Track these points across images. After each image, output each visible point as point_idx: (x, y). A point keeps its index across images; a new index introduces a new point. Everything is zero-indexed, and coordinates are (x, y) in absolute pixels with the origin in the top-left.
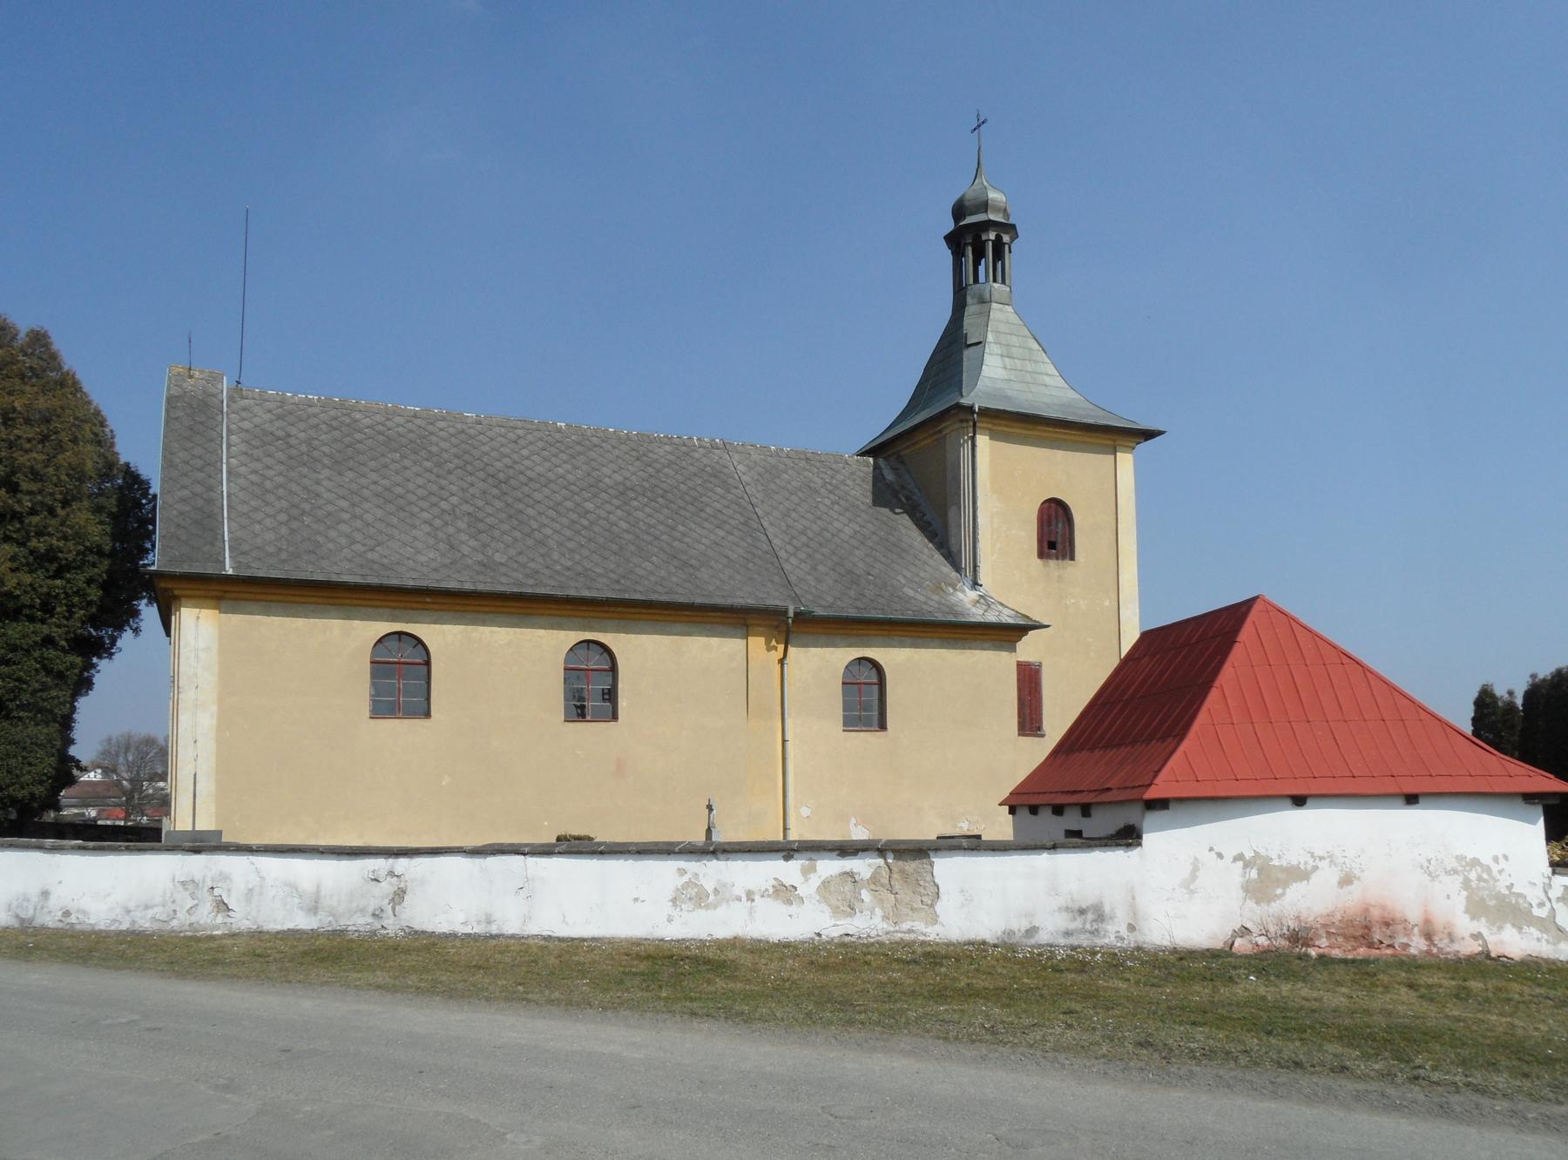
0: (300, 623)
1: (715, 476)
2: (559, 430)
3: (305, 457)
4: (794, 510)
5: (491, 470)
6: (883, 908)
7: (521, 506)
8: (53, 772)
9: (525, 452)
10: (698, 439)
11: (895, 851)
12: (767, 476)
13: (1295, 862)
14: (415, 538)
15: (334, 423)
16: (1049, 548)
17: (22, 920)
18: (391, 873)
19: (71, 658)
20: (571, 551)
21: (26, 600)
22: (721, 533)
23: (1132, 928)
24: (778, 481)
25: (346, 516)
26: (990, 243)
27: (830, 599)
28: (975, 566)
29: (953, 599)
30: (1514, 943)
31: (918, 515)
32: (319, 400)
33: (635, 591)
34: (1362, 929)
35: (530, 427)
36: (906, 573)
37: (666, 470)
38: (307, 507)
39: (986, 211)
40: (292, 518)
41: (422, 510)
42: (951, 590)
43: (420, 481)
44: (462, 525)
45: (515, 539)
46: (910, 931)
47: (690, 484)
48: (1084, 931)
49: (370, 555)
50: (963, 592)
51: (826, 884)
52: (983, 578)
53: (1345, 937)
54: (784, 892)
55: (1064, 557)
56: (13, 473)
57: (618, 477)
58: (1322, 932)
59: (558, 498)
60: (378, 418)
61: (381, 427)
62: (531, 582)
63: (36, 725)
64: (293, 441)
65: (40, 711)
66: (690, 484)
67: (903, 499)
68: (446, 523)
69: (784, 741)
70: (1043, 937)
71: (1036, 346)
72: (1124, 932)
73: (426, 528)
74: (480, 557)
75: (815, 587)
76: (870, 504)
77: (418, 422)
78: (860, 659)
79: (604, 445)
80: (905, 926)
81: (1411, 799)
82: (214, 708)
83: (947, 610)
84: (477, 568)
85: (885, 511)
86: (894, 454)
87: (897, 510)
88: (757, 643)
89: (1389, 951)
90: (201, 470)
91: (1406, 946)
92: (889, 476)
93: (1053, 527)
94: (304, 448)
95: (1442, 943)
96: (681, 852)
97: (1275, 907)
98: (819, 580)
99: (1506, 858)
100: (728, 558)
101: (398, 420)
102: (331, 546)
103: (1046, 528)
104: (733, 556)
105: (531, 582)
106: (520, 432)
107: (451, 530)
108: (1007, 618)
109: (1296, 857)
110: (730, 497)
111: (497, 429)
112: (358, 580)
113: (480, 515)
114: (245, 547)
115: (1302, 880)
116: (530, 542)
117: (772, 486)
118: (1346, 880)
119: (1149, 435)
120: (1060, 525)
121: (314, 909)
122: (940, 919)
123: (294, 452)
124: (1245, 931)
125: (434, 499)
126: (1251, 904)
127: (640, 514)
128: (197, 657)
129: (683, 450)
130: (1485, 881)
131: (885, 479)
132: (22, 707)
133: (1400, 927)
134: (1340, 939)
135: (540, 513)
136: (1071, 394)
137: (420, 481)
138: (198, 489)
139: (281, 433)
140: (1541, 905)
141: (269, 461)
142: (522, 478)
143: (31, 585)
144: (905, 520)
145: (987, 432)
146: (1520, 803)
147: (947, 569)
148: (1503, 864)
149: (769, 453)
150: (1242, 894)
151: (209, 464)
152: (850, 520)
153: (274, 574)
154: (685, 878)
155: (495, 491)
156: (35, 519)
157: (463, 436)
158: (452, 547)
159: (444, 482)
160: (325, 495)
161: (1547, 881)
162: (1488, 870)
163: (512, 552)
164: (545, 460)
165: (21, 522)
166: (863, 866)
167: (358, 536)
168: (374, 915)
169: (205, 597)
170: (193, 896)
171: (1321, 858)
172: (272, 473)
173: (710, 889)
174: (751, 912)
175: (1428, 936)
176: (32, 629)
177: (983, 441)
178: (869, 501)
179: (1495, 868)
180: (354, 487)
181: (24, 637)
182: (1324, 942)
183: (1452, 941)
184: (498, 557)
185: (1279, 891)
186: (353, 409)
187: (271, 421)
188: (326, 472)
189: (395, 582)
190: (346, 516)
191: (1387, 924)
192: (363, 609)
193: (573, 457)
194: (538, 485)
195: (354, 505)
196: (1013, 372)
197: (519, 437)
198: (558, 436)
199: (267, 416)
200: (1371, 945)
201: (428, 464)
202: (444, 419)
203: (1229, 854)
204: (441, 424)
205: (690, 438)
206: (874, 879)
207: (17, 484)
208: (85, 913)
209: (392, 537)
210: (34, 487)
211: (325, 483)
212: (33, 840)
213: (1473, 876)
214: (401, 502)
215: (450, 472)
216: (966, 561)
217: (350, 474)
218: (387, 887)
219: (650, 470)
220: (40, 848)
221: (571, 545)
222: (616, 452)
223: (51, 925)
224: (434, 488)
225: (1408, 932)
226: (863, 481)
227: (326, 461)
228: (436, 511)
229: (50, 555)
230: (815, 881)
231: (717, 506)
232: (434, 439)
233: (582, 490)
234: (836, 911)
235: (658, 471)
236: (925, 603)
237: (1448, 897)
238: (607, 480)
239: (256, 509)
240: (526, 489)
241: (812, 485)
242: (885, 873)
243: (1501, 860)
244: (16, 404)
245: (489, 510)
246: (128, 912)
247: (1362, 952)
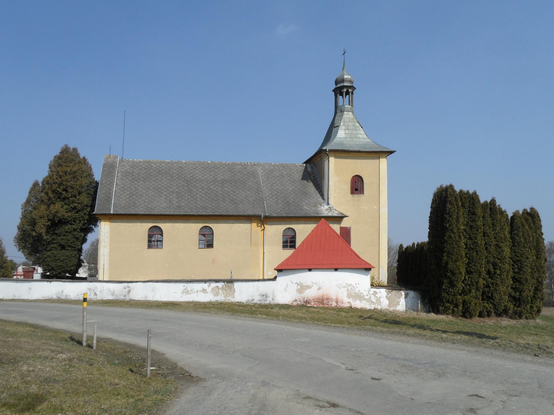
0: (130, 224)
1: (252, 175)
2: (208, 164)
3: (137, 179)
4: (275, 183)
5: (186, 178)
6: (224, 294)
7: (192, 188)
8: (76, 264)
9: (197, 172)
10: (250, 163)
11: (227, 281)
12: (269, 173)
13: (308, 284)
14: (161, 200)
15: (146, 167)
16: (355, 191)
17: (58, 297)
18: (128, 287)
19: (79, 234)
20: (203, 201)
21: (70, 219)
22: (249, 193)
23: (273, 299)
24: (272, 174)
25: (144, 195)
26: (345, 93)
27: (279, 211)
29: (319, 209)
30: (358, 304)
31: (316, 182)
32: (143, 161)
33: (218, 212)
34: (321, 300)
35: (200, 163)
36: (306, 201)
37: (238, 174)
38: (135, 193)
39: (344, 82)
40: (130, 196)
41: (165, 191)
42: (320, 206)
43: (166, 183)
44: (175, 195)
45: (188, 199)
46: (229, 300)
47: (244, 178)
48: (263, 300)
49: (148, 206)
50: (324, 206)
51: (213, 289)
53: (318, 302)
54: (204, 291)
55: (360, 193)
56: (66, 188)
57: (222, 177)
58: (313, 301)
59: (203, 185)
60: (158, 165)
61: (158, 168)
62: (189, 211)
63: (72, 251)
64: (134, 174)
65: (73, 247)
66: (244, 178)
67: (312, 177)
68: (170, 195)
69: (264, 253)
70: (255, 302)
71: (358, 125)
72: (271, 300)
73: (165, 197)
74: (177, 204)
75: (276, 207)
76: (301, 179)
77: (169, 165)
78: (289, 228)
79: (221, 167)
80: (228, 299)
81: (336, 270)
82: (109, 247)
83: (316, 212)
84: (176, 208)
85: (305, 181)
86: (312, 162)
87: (309, 181)
88: (254, 225)
89: (327, 306)
90: (109, 185)
91: (331, 304)
92: (309, 169)
93: (357, 184)
94: (137, 176)
95: (340, 304)
96: (183, 282)
97: (302, 295)
98: (277, 205)
99: (359, 284)
100: (249, 200)
101: (164, 165)
102: (139, 204)
103: (354, 184)
104: (250, 199)
105: (189, 211)
106: (197, 165)
107: (171, 197)
108: (335, 214)
109: (308, 283)
110: (255, 181)
111: (190, 165)
112: (144, 213)
113: (180, 192)
114: (117, 205)
115: (309, 288)
116: (192, 199)
117: (270, 176)
118: (319, 289)
119: (391, 152)
120: (359, 183)
121: (113, 295)
122: (235, 297)
123: (134, 177)
124: (296, 300)
125: (168, 188)
126: (298, 294)
127: (226, 188)
128: (104, 234)
129: (244, 166)
130: (353, 289)
131: (307, 171)
132: (69, 246)
133: (330, 300)
134: (317, 303)
135: (197, 190)
136: (368, 140)
137: (166, 183)
138: (108, 190)
139: (131, 172)
140: (367, 295)
141: (127, 180)
142: (195, 180)
143: (71, 216)
144: (311, 184)
145: (334, 156)
146: (364, 271)
147: (320, 199)
148: (358, 285)
149: (271, 165)
150: (296, 292)
151: (111, 183)
152: (292, 185)
153: (123, 213)
154: (185, 288)
155: (186, 184)
156: (71, 199)
157: (180, 168)
158: (171, 202)
159: (172, 183)
160: (140, 189)
161: (369, 290)
162: (354, 287)
163: (187, 202)
164: (203, 173)
165: (69, 199)
166: (220, 285)
167: (146, 200)
168: (124, 296)
169: (106, 219)
170: (90, 292)
171: (314, 283)
172: (127, 184)
173: (189, 290)
174: (198, 295)
175: (337, 302)
176: (71, 227)
177: (332, 160)
178: (300, 179)
179: (355, 286)
180: (148, 186)
181: (69, 229)
182: (313, 303)
183: (342, 303)
184: (183, 204)
185: (304, 291)
186: (152, 163)
187: (129, 169)
188: (141, 183)
189: (153, 213)
190: (144, 195)
191: (328, 299)
192: (146, 220)
193: (211, 172)
194: (198, 182)
195: (147, 191)
196: (348, 135)
197: (196, 167)
198: (207, 166)
199: (129, 167)
200: (323, 304)
201: (169, 178)
202: (176, 163)
203: (294, 282)
204: (175, 165)
205: (248, 163)
206: (222, 288)
207: (67, 190)
208: (70, 296)
209: (155, 200)
210: (72, 190)
211: (140, 186)
213: (349, 288)
214: (159, 189)
215: (174, 180)
216: (326, 197)
217: (148, 182)
218: (127, 290)
219: (233, 174)
220: (61, 281)
221: (203, 199)
222: (224, 169)
223: (63, 298)
224: (169, 185)
225: (332, 301)
226: (300, 172)
227: (142, 179)
228: (168, 192)
229: (75, 208)
230: (211, 288)
231: (250, 184)
232: (172, 170)
233: (211, 182)
234: (214, 295)
235: (235, 175)
236: (309, 211)
237: (343, 293)
238: (219, 178)
239: (121, 195)
240: (195, 183)
241: (283, 175)
242: (224, 286)
243: (358, 285)
244: (68, 169)
245: (183, 190)
246: (78, 295)
247: (321, 305)
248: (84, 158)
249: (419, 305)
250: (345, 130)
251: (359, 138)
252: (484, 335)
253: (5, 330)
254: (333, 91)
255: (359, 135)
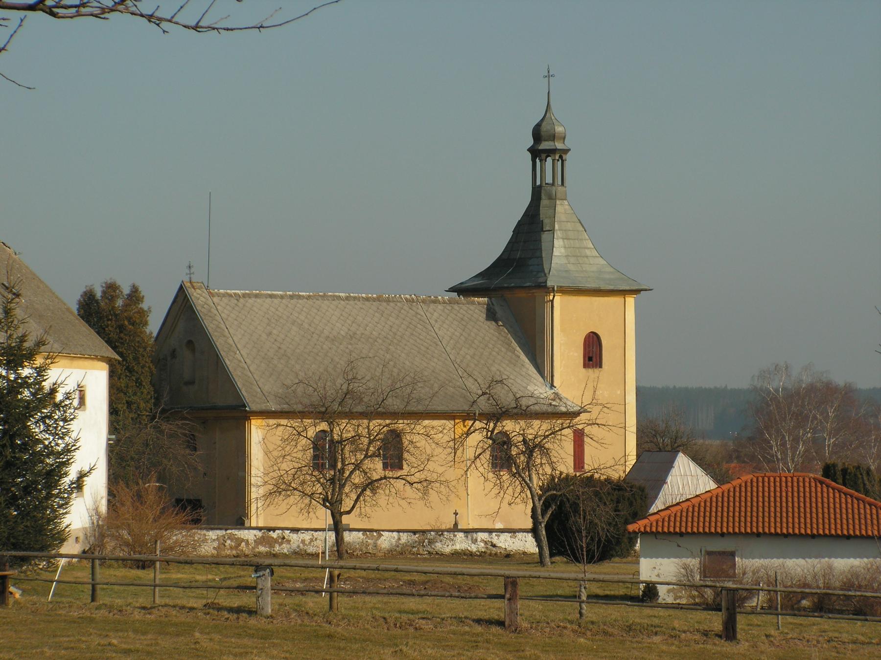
28: (552, 376)
52: (556, 383)
71: (581, 229)
103: (587, 348)
212: (544, 532)
248: (143, 296)
249: (374, 565)
250: (563, 239)
251: (587, 257)
252: (229, 613)
253: (714, 654)
254: (528, 150)
255: (586, 250)
